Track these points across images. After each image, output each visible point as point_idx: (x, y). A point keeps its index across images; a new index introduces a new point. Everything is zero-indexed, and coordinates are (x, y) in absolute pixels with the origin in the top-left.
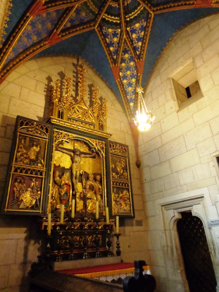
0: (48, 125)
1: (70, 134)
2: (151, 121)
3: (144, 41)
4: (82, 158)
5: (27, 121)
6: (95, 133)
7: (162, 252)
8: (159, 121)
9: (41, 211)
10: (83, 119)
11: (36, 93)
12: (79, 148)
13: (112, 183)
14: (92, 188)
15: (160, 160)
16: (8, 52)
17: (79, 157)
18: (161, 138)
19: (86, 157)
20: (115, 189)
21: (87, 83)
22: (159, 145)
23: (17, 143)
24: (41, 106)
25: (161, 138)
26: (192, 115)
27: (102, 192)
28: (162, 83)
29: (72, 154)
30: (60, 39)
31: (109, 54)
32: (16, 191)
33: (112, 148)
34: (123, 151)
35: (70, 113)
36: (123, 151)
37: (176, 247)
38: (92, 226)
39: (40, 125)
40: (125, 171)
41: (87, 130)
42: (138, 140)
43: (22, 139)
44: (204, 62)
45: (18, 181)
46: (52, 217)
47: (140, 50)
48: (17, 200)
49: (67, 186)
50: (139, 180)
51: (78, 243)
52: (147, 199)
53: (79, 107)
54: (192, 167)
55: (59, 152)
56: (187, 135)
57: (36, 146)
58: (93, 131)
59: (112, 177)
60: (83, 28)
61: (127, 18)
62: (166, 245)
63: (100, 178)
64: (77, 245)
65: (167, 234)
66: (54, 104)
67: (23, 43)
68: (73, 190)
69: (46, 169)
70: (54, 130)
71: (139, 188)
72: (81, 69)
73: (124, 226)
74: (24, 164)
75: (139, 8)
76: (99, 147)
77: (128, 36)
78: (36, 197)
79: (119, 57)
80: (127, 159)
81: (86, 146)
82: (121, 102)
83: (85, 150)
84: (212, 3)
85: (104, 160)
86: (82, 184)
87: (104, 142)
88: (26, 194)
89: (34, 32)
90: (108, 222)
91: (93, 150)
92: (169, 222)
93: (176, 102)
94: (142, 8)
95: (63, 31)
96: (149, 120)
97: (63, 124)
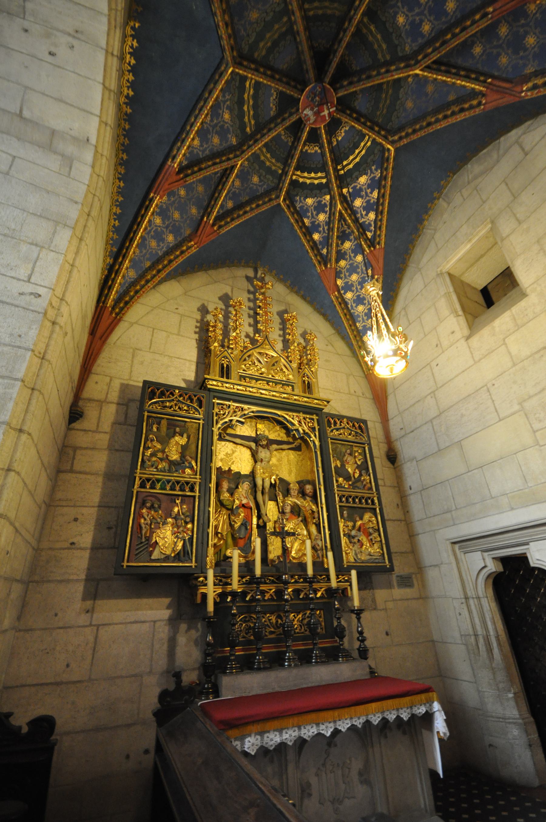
0: (202, 394)
1: (246, 407)
2: (406, 350)
3: (381, 208)
4: (275, 452)
5: (162, 389)
6: (295, 400)
7: (463, 647)
8: (428, 364)
9: (193, 564)
10: (270, 376)
11: (180, 337)
12: (267, 433)
13: (337, 499)
14: (296, 511)
15: (438, 444)
16: (122, 268)
17: (266, 450)
18: (435, 398)
19: (282, 449)
20: (344, 510)
21: (274, 309)
22: (433, 413)
23: (144, 431)
24: (190, 361)
25: (435, 398)
26: (504, 340)
27: (319, 519)
28: (425, 286)
29: (253, 445)
30: (215, 233)
31: (312, 248)
32: (143, 526)
33: (332, 428)
34: (356, 433)
35: (243, 366)
36: (356, 433)
37: (497, 637)
38: (302, 591)
39: (186, 395)
40: (363, 472)
41: (277, 395)
42: (387, 408)
43: (154, 424)
44: (520, 222)
45: (148, 505)
46: (215, 576)
47: (372, 228)
48: (147, 542)
49: (246, 509)
50: (397, 488)
51: (275, 629)
52: (418, 527)
53: (260, 353)
54: (517, 454)
55: (227, 443)
56: (496, 386)
57: (180, 435)
58: (290, 397)
59: (338, 486)
60: (258, 206)
61: (341, 170)
62: (471, 633)
63: (312, 491)
64: (271, 633)
65: (473, 607)
66: (212, 352)
67: (150, 250)
68: (259, 517)
69: (200, 479)
70: (214, 401)
71: (398, 505)
72: (260, 284)
73: (373, 589)
74: (157, 471)
75: (362, 144)
76: (306, 428)
77: (345, 205)
78: (184, 537)
79: (332, 249)
80: (367, 448)
81: (280, 427)
82: (344, 337)
83: (279, 435)
84: (522, 92)
85: (319, 453)
86: (278, 504)
87: (315, 417)
88: (163, 531)
89: (167, 227)
90: (334, 583)
91: (294, 434)
92: (474, 582)
93: (462, 320)
94: (369, 144)
95: (219, 218)
96: (399, 349)
97: (231, 388)
